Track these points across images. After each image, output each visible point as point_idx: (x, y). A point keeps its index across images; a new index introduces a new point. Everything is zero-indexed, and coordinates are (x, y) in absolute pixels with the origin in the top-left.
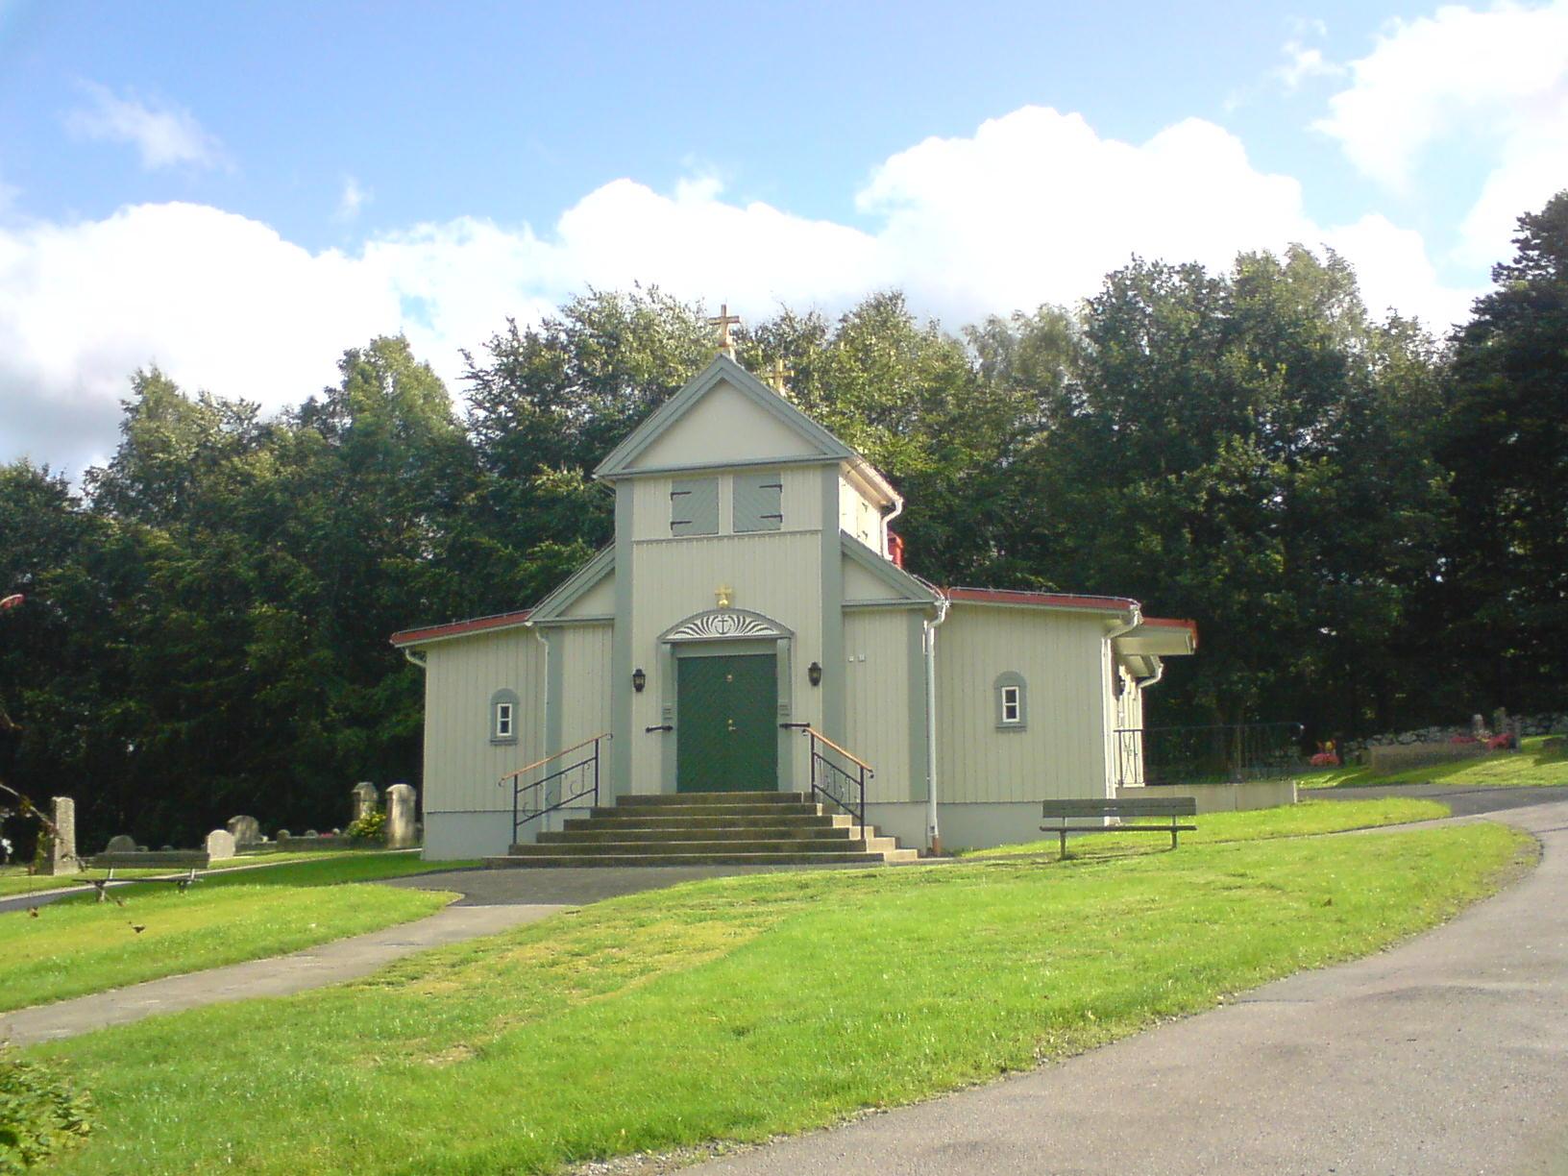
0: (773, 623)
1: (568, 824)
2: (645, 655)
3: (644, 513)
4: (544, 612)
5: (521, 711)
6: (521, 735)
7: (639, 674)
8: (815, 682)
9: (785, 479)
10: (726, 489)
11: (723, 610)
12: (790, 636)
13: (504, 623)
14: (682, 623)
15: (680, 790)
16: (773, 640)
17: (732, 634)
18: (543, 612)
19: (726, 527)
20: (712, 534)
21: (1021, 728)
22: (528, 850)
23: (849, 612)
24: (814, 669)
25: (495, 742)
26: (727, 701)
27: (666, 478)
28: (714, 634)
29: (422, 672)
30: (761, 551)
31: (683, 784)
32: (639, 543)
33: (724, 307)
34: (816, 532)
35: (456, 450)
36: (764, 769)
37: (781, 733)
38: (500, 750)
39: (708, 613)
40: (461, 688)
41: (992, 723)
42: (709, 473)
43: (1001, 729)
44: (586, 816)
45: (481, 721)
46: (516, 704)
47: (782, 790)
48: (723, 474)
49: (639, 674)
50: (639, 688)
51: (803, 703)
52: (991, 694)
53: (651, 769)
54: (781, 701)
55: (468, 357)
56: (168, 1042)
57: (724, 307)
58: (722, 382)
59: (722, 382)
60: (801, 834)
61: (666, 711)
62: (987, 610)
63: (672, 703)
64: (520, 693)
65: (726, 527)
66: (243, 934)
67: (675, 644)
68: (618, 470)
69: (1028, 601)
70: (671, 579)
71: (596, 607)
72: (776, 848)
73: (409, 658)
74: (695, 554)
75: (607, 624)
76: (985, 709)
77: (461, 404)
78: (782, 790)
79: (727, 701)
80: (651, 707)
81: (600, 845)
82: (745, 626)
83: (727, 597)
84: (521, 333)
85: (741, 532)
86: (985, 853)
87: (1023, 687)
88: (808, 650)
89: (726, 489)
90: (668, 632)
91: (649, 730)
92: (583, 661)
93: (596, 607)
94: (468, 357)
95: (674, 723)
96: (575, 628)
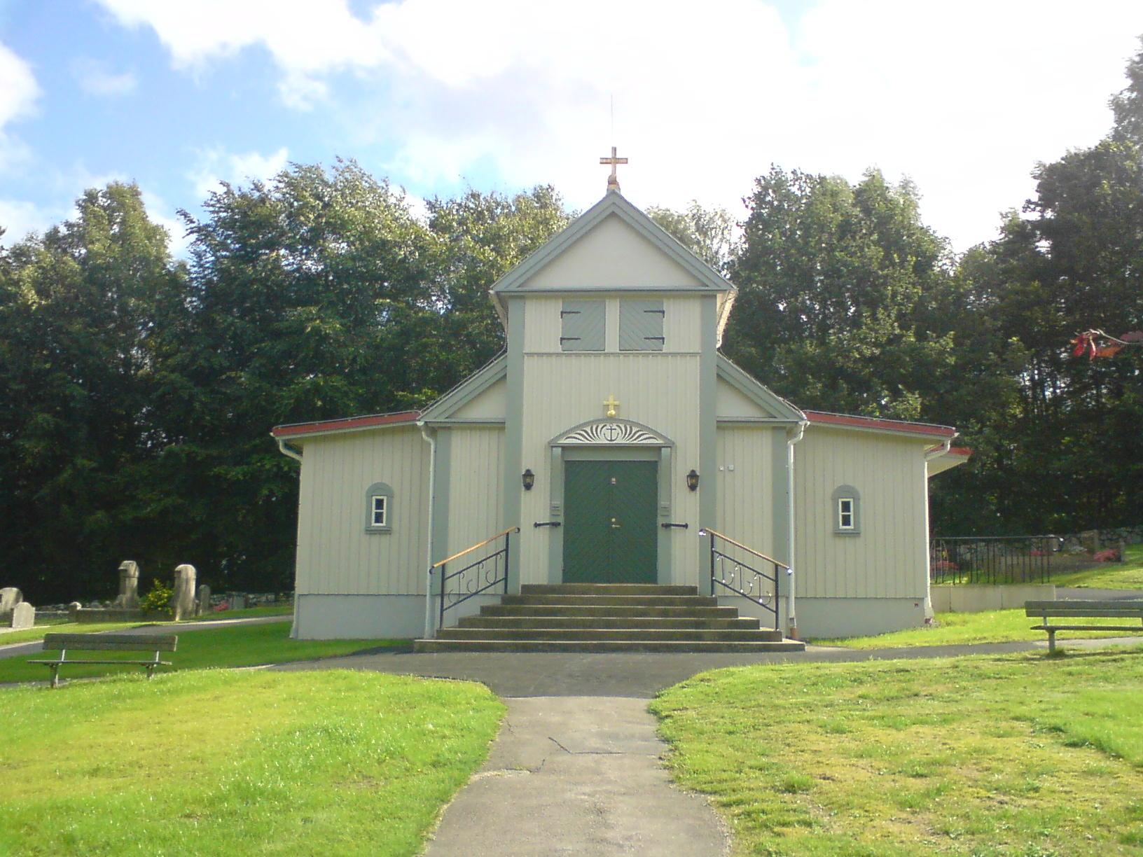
0: (658, 435)
1: (484, 610)
2: (534, 456)
3: (535, 329)
4: (437, 412)
5: (396, 501)
6: (395, 526)
7: (529, 474)
8: (693, 488)
9: (668, 306)
10: (613, 312)
11: (611, 419)
12: (671, 445)
13: (390, 421)
14: (571, 430)
15: (565, 580)
16: (658, 449)
17: (620, 441)
18: (436, 413)
19: (612, 344)
20: (598, 350)
21: (855, 534)
22: (448, 635)
23: (724, 426)
24: (693, 475)
25: (370, 532)
26: (611, 502)
27: (557, 298)
28: (602, 440)
29: (295, 468)
30: (642, 368)
31: (568, 575)
32: (531, 355)
33: (614, 150)
34: (693, 354)
35: (174, 283)
36: (643, 562)
37: (661, 533)
38: (375, 539)
39: (597, 421)
40: (335, 482)
41: (829, 526)
42: (599, 295)
43: (838, 534)
44: (496, 602)
45: (358, 510)
46: (391, 497)
47: (662, 583)
48: (611, 297)
49: (529, 474)
50: (528, 487)
51: (681, 505)
52: (829, 504)
53: (538, 561)
54: (662, 503)
55: (185, 215)
56: (69, 809)
57: (614, 150)
58: (613, 215)
59: (613, 215)
60: (709, 628)
61: (554, 508)
62: (836, 433)
63: (559, 502)
64: (396, 490)
65: (612, 344)
66: (211, 719)
67: (565, 448)
68: (513, 288)
69: (351, 425)
70: (563, 391)
71: (487, 409)
72: (698, 637)
73: (283, 450)
74: (584, 368)
75: (498, 426)
76: (825, 514)
77: (180, 248)
78: (662, 583)
79: (611, 502)
80: (539, 505)
81: (511, 632)
82: (631, 435)
83: (616, 407)
84: (237, 193)
85: (625, 350)
86: (865, 643)
87: (857, 499)
88: (686, 459)
89: (613, 312)
90: (561, 436)
91: (536, 525)
92: (471, 463)
93: (487, 409)
94: (185, 215)
95: (561, 519)
96: (462, 429)
